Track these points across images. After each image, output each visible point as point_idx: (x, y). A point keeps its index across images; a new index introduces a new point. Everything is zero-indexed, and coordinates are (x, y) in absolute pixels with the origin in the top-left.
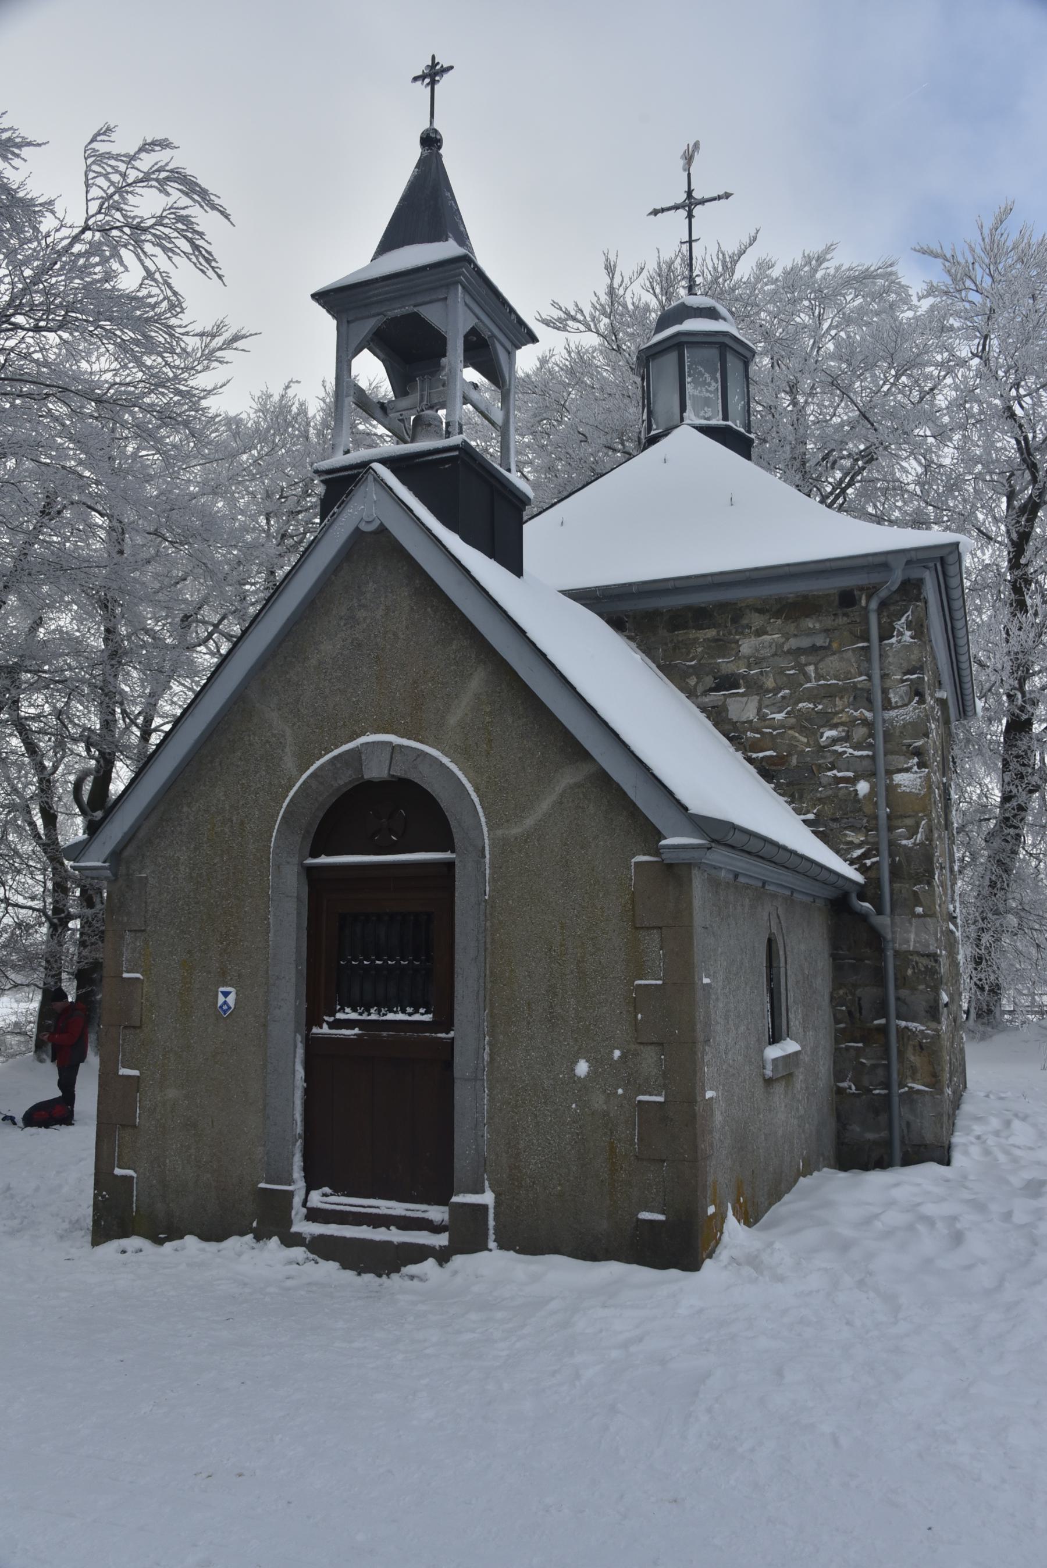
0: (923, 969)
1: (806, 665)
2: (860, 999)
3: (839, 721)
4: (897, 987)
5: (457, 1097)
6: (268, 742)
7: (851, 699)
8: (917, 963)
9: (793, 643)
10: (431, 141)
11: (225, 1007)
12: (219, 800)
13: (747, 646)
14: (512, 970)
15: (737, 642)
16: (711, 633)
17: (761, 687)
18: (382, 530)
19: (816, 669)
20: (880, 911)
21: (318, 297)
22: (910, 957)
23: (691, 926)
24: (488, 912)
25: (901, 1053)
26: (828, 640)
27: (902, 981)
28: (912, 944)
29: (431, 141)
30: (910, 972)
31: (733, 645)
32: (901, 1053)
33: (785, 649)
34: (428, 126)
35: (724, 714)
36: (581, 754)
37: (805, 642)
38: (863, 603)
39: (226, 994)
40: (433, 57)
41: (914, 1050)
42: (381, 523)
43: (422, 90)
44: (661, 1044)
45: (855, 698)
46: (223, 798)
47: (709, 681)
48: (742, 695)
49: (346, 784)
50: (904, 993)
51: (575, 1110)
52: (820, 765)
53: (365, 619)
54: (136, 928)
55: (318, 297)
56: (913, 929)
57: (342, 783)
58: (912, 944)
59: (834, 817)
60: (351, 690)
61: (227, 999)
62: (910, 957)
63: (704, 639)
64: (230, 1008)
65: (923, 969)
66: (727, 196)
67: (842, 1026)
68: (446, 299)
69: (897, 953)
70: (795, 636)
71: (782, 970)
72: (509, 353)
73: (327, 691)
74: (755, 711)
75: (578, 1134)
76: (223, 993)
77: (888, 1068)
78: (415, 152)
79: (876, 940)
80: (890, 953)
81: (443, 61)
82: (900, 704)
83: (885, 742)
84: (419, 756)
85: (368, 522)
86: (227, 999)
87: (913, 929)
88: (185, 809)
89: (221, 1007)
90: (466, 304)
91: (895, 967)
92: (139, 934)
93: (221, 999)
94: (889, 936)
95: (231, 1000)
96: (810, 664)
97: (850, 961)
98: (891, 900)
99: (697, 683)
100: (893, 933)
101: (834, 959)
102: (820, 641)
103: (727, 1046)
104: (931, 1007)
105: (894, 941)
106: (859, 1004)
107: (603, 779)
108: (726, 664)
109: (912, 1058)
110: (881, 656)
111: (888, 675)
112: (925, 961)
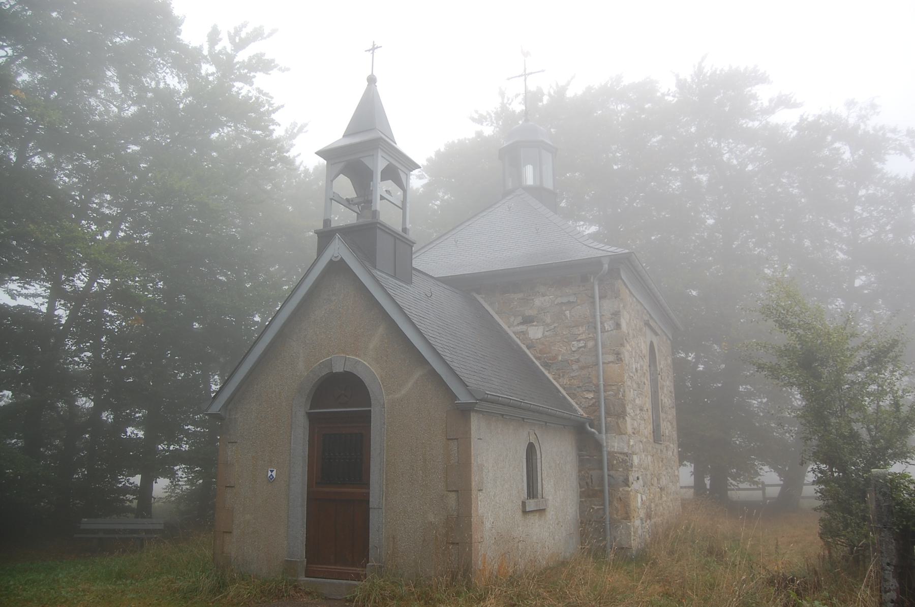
0: (621, 460)
1: (565, 311)
2: (591, 476)
3: (581, 338)
4: (608, 470)
5: (371, 517)
6: (291, 356)
7: (587, 327)
8: (618, 458)
9: (559, 300)
10: (372, 80)
11: (271, 477)
12: (270, 382)
13: (538, 301)
14: (396, 459)
15: (533, 300)
16: (521, 295)
17: (544, 322)
18: (342, 260)
19: (570, 313)
20: (600, 432)
21: (316, 153)
22: (615, 455)
23: (470, 438)
24: (385, 433)
25: (611, 502)
26: (575, 299)
27: (611, 467)
28: (616, 448)
29: (372, 80)
30: (615, 462)
31: (531, 301)
32: (611, 502)
33: (556, 303)
34: (370, 73)
35: (527, 336)
36: (423, 361)
37: (565, 300)
38: (592, 280)
39: (272, 471)
40: (374, 42)
41: (618, 501)
42: (342, 257)
43: (369, 54)
44: (457, 491)
45: (588, 327)
46: (272, 381)
47: (520, 319)
48: (536, 326)
49: (325, 375)
50: (612, 473)
51: (71, 401)
52: (572, 361)
53: (335, 300)
54: (233, 441)
55: (316, 153)
56: (616, 441)
57: (323, 374)
58: (616, 448)
59: (579, 386)
60: (328, 332)
61: (272, 474)
62: (615, 455)
63: (518, 299)
64: (273, 477)
65: (621, 460)
66: (543, 71)
67: (583, 489)
68: (373, 155)
69: (609, 453)
70: (561, 296)
71: (539, 461)
72: (407, 175)
73: (318, 333)
74: (542, 334)
75: (422, 532)
76: (270, 471)
77: (604, 509)
78: (365, 84)
79: (599, 446)
80: (605, 454)
81: (378, 44)
82: (609, 329)
83: (602, 348)
84: (356, 362)
85: (336, 257)
86: (272, 474)
87: (616, 441)
88: (255, 386)
89: (270, 477)
90: (382, 157)
91: (608, 459)
92: (234, 444)
93: (270, 473)
94: (605, 444)
95: (274, 474)
96: (567, 310)
97: (587, 457)
98: (606, 426)
99: (514, 320)
100: (607, 442)
101: (579, 456)
102: (572, 299)
103: (495, 493)
104: (625, 479)
105: (607, 446)
106: (591, 479)
107: (433, 373)
108: (529, 312)
109: (616, 505)
110: (600, 306)
111: (604, 315)
112: (622, 456)
